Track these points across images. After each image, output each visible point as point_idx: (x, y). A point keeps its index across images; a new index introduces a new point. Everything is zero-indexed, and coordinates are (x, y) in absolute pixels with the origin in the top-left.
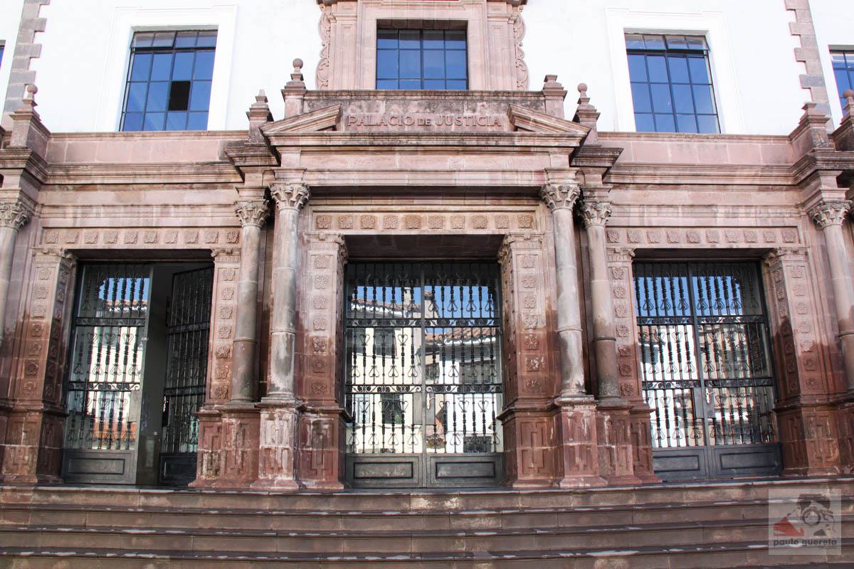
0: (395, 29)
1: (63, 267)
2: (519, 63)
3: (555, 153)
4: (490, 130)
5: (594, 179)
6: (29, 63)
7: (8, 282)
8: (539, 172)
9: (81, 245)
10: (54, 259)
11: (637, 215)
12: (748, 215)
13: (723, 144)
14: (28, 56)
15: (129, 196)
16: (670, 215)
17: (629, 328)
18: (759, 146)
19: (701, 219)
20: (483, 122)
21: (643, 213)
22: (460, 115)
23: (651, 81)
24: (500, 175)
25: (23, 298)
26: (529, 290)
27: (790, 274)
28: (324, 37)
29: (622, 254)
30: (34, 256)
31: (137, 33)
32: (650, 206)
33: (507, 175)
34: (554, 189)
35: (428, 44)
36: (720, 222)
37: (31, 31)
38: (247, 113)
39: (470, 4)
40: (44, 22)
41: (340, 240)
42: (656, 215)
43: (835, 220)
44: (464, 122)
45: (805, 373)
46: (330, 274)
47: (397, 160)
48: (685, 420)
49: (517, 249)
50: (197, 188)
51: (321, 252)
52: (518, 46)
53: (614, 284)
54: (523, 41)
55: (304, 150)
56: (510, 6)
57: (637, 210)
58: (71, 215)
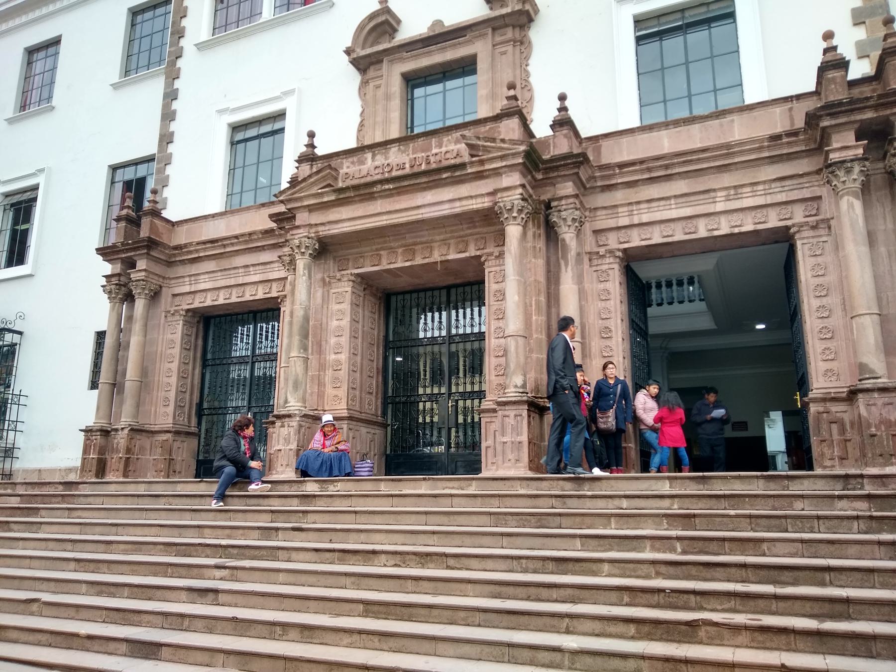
0: (422, 78)
1: (186, 323)
2: (524, 83)
3: (505, 173)
4: (453, 162)
5: (564, 188)
6: (165, 169)
7: (143, 338)
8: (489, 194)
9: (196, 305)
10: (178, 318)
11: (627, 214)
12: (754, 194)
13: (731, 118)
14: (164, 164)
15: (225, 263)
16: (661, 208)
17: (613, 329)
18: (778, 110)
19: (698, 207)
20: (448, 156)
21: (632, 211)
22: (429, 153)
23: (462, 113)
24: (458, 204)
25: (159, 349)
26: (499, 303)
27: (808, 253)
28: (363, 100)
29: (608, 256)
30: (166, 317)
31: (635, 17)
32: (638, 203)
33: (464, 203)
34: (500, 208)
35: (450, 84)
36: (720, 207)
37: (165, 143)
38: (551, 126)
39: (477, 37)
40: (172, 134)
41: (353, 278)
42: (646, 211)
43: (847, 182)
44: (432, 159)
45: (821, 363)
46: (345, 307)
47: (379, 206)
48: (465, 415)
49: (489, 267)
50: (268, 249)
51: (339, 290)
52: (524, 66)
53: (599, 286)
54: (530, 62)
55: (311, 209)
56: (517, 30)
57: (625, 209)
58: (188, 283)
